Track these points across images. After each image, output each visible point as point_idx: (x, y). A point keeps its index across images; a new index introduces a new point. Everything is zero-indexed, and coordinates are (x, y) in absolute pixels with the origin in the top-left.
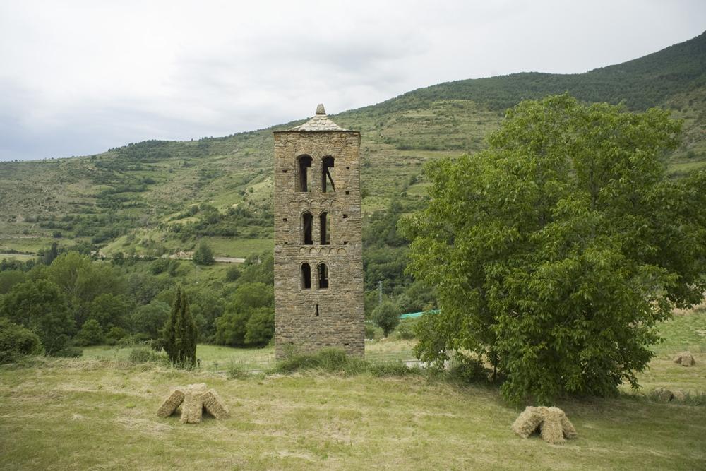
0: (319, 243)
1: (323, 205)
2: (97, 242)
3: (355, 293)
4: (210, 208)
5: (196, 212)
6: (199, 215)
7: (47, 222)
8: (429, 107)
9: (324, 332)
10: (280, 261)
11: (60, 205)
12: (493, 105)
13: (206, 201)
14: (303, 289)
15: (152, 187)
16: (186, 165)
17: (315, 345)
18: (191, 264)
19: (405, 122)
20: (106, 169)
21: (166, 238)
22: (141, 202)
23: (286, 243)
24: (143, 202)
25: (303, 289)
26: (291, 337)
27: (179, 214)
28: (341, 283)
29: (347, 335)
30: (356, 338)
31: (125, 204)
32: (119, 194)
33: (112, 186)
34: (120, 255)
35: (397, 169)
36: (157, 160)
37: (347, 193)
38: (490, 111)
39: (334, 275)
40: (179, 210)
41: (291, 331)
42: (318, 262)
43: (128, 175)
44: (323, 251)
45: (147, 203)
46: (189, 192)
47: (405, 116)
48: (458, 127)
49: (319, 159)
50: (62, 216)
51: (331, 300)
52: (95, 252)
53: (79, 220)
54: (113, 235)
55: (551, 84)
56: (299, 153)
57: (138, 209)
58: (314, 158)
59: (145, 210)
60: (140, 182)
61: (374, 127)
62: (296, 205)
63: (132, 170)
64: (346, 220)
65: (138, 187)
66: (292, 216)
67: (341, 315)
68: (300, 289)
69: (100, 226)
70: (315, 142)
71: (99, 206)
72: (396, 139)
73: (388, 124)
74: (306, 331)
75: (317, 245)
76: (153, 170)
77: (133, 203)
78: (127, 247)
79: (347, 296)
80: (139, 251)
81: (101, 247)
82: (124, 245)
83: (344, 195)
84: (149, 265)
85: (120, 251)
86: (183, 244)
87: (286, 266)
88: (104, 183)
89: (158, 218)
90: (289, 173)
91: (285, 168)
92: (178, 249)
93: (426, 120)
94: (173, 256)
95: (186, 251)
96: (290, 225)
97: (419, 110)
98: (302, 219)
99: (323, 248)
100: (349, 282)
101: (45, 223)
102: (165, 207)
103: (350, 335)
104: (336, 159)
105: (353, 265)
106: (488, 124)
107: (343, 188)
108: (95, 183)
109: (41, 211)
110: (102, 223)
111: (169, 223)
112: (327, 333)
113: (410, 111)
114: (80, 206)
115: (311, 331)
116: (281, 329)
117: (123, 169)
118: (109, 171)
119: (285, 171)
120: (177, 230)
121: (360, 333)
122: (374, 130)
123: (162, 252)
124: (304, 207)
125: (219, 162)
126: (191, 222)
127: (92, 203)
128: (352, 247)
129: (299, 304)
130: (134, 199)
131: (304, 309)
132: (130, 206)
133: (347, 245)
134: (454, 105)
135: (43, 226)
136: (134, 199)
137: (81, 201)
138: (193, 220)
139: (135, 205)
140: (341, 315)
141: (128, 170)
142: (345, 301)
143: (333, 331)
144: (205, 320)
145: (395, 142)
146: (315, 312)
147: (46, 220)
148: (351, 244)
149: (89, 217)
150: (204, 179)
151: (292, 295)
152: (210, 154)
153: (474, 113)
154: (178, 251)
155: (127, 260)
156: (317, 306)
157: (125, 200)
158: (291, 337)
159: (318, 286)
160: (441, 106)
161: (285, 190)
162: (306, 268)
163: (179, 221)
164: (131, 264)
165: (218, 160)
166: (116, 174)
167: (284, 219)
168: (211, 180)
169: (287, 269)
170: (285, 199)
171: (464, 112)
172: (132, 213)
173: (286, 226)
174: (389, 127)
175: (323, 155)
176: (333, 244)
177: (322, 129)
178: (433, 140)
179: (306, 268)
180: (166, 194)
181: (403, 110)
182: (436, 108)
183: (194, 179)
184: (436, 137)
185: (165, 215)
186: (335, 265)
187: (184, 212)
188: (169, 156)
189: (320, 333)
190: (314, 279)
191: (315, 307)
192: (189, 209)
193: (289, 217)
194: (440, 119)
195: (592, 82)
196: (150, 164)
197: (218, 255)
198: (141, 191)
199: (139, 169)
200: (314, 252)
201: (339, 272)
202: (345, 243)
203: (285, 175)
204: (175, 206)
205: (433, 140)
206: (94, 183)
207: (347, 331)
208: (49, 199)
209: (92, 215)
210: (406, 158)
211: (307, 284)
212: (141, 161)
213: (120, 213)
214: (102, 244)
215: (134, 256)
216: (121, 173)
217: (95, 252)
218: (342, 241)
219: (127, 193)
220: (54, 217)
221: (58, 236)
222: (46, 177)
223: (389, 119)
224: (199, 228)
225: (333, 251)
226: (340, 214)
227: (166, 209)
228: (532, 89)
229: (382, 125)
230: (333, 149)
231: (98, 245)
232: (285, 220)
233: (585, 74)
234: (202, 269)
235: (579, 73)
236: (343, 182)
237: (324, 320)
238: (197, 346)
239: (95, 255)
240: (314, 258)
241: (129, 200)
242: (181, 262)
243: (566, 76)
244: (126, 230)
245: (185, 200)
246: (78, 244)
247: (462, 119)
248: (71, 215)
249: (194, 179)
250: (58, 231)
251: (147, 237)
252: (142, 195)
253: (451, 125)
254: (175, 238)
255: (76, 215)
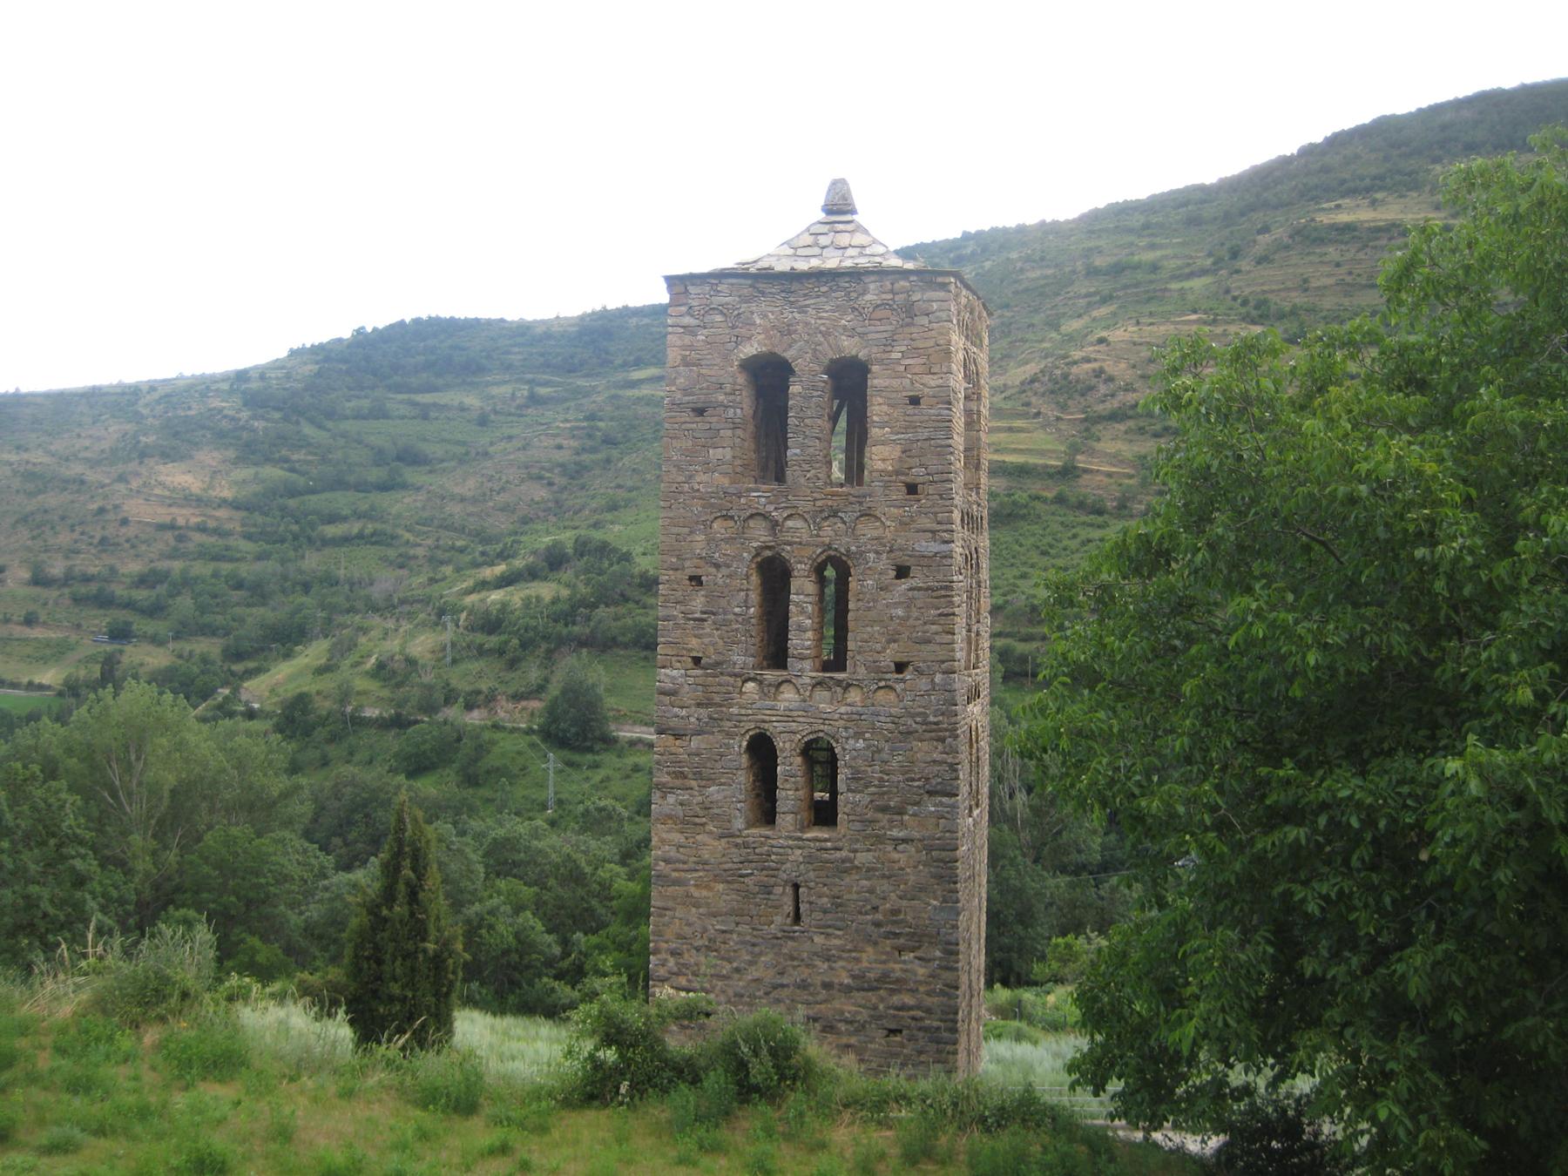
0: (807, 665)
2: (239, 656)
3: (930, 849)
4: (604, 549)
5: (561, 563)
6: (567, 575)
7: (93, 588)
8: (1416, 186)
9: (818, 980)
11: (129, 531)
13: (596, 526)
14: (749, 825)
15: (411, 475)
16: (534, 400)
18: (533, 745)
19: (1321, 241)
20: (277, 415)
21: (457, 655)
22: (379, 526)
24: (388, 528)
25: (749, 825)
27: (500, 569)
28: (884, 809)
30: (929, 1011)
31: (331, 531)
32: (314, 498)
33: (292, 470)
34: (301, 702)
36: (440, 382)
37: (912, 489)
39: (855, 777)
40: (503, 556)
42: (804, 730)
43: (344, 435)
45: (400, 532)
46: (540, 493)
47: (1324, 219)
50: (134, 567)
51: (845, 868)
52: (227, 691)
53: (186, 582)
54: (287, 638)
56: (750, 350)
57: (374, 549)
58: (798, 365)
59: (392, 553)
60: (380, 458)
63: (358, 416)
64: (904, 585)
65: (375, 474)
66: (717, 566)
67: (877, 924)
68: (739, 823)
69: (248, 605)
70: (802, 309)
71: (248, 537)
72: (1287, 307)
73: (1258, 250)
74: (754, 973)
75: (805, 670)
76: (425, 417)
77: (356, 528)
78: (328, 675)
80: (365, 693)
81: (250, 674)
82: (321, 671)
83: (899, 494)
84: (392, 742)
85: (305, 689)
86: (509, 675)
87: (696, 743)
88: (267, 460)
89: (432, 581)
90: (712, 419)
92: (493, 690)
94: (476, 713)
95: (517, 697)
97: (1379, 196)
98: (755, 579)
99: (819, 683)
100: (911, 810)
101: (83, 590)
102: (459, 543)
103: (908, 1000)
105: (925, 746)
107: (897, 473)
108: (239, 461)
109: (78, 552)
110: (258, 592)
111: (469, 600)
112: (827, 986)
113: (1346, 202)
114: (191, 534)
115: (769, 976)
116: (671, 962)
117: (330, 415)
118: (286, 419)
119: (700, 412)
120: (491, 624)
122: (1204, 272)
123: (439, 696)
124: (759, 534)
125: (645, 391)
126: (538, 598)
127: (228, 526)
128: (923, 684)
129: (731, 877)
130: (359, 516)
131: (747, 895)
132: (346, 540)
133: (908, 675)
135: (77, 600)
136: (359, 516)
137: (195, 520)
138: (546, 591)
139: (360, 536)
141: (347, 418)
144: (549, 938)
145: (1281, 316)
146: (789, 908)
147: (87, 579)
149: (215, 575)
150: (594, 450)
151: (711, 847)
152: (618, 361)
154: (490, 699)
155: (323, 721)
156: (796, 887)
157: (332, 519)
162: (762, 750)
163: (496, 596)
164: (333, 738)
165: (641, 382)
166: (308, 430)
167: (691, 578)
168: (615, 453)
172: (349, 564)
173: (698, 602)
174: (1262, 260)
176: (857, 668)
177: (832, 264)
179: (762, 750)
180: (463, 500)
181: (1314, 199)
183: (560, 447)
185: (458, 570)
186: (861, 744)
187: (519, 563)
188: (481, 370)
190: (791, 793)
191: (789, 890)
192: (534, 553)
193: (708, 574)
196: (419, 398)
197: (621, 718)
198: (384, 487)
199: (379, 413)
200: (788, 696)
201: (875, 772)
202: (900, 667)
203: (699, 425)
204: (487, 540)
206: (237, 462)
207: (899, 985)
208: (102, 510)
209: (226, 567)
211: (767, 813)
212: (389, 388)
213: (312, 561)
214: (251, 665)
215: (349, 709)
216: (320, 427)
217: (227, 691)
218: (888, 658)
219: (338, 495)
220: (113, 570)
221: (120, 634)
222: (99, 439)
223: (1265, 230)
224: (568, 617)
225: (854, 696)
226: (884, 564)
227: (462, 550)
229: (1235, 254)
231: (238, 668)
232: (696, 580)
234: (570, 764)
236: (897, 453)
237: (818, 939)
238: (456, 1014)
239: (226, 698)
240: (788, 717)
241: (345, 519)
242: (498, 736)
244: (329, 620)
245: (525, 521)
246: (180, 662)
248: (163, 565)
249: (560, 447)
250: (122, 615)
251: (393, 645)
252: (382, 500)
254: (481, 652)
255: (177, 566)
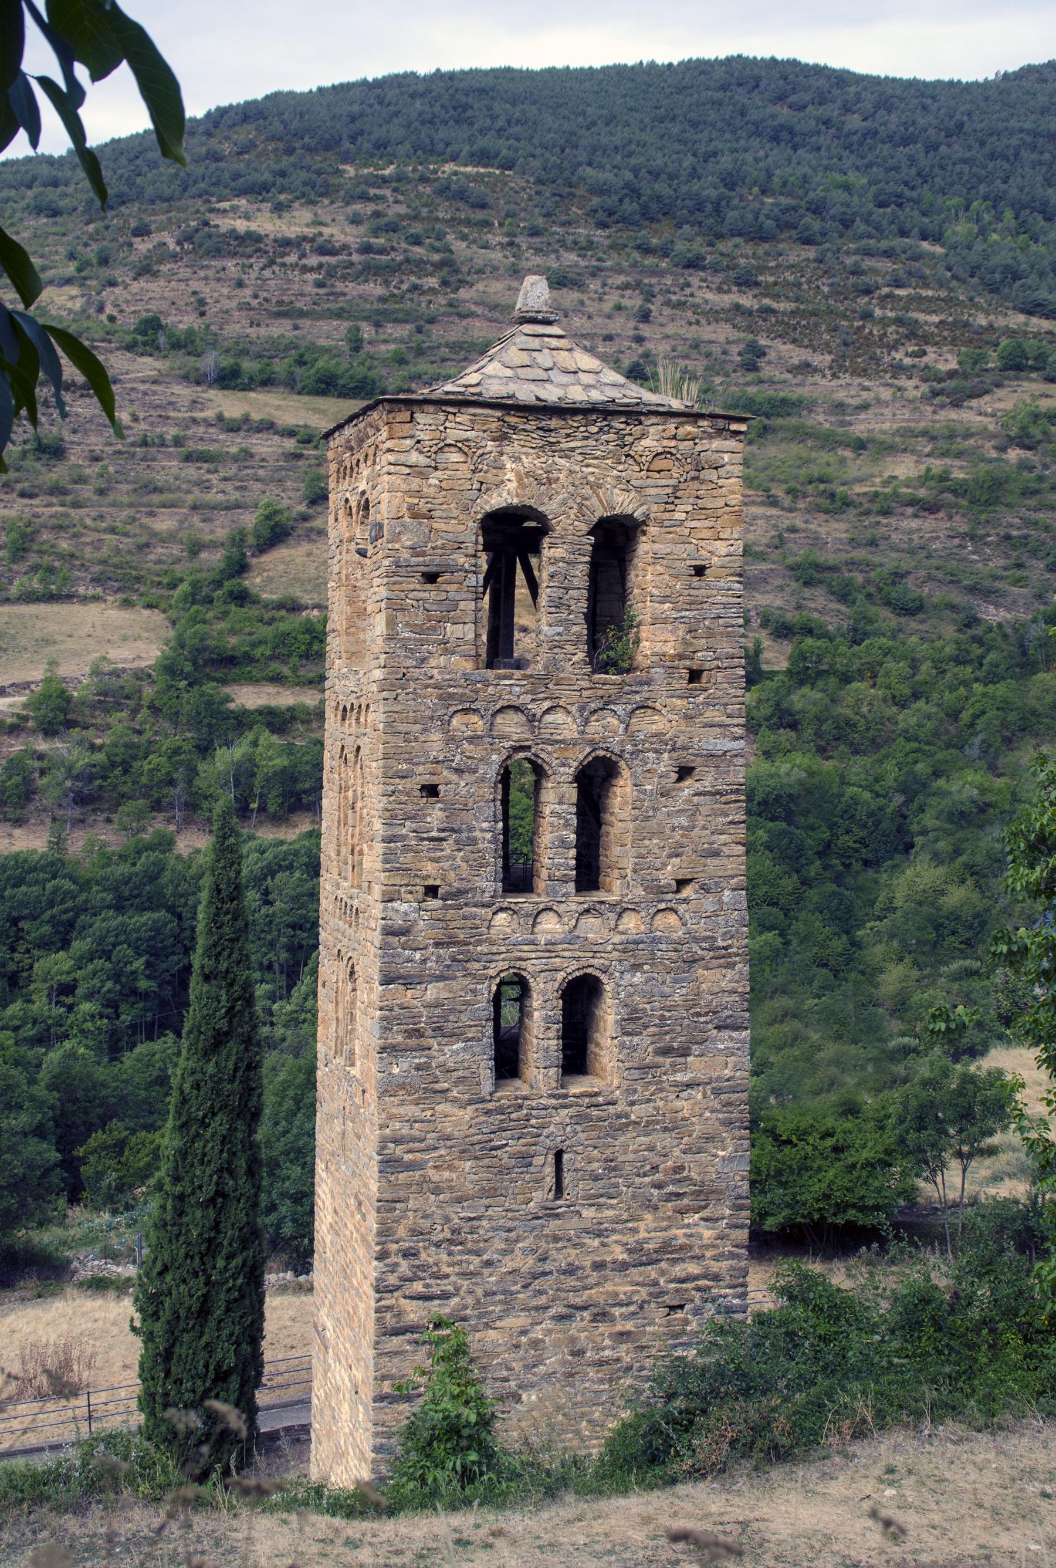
1: (594, 727)
3: (717, 1092)
8: (327, 191)
10: (409, 968)
12: (611, 201)
17: (548, 1324)
19: (217, 252)
23: (432, 891)
26: (445, 1296)
29: (678, 1270)
30: (716, 1278)
35: (191, 471)
37: (695, 676)
38: (603, 225)
41: (447, 1270)
42: (570, 968)
44: (590, 921)
47: (225, 224)
48: (463, 294)
49: (585, 528)
55: (854, 122)
56: (496, 501)
61: (71, 269)
62: (478, 724)
64: (689, 786)
66: (459, 771)
67: (659, 1186)
79: (684, 1106)
90: (448, 587)
91: (431, 561)
93: (323, 251)
96: (450, 811)
103: (693, 1268)
104: (653, 530)
106: (594, 285)
107: (681, 657)
112: (598, 1266)
116: (404, 1267)
119: (431, 578)
121: (732, 1256)
128: (709, 904)
134: (444, 191)
140: (659, 1186)
142: (674, 1126)
143: (623, 1256)
146: (550, 1181)
148: (705, 889)
153: (535, 232)
156: (559, 1155)
158: (445, 1296)
159: (563, 1067)
160: (387, 192)
161: (433, 662)
167: (423, 788)
169: (437, 1005)
170: (431, 698)
171: (486, 224)
173: (435, 816)
175: (600, 513)
178: (356, 345)
182: (364, 197)
184: (367, 331)
189: (571, 1270)
191: (551, 1158)
194: (381, 251)
195: (1013, 123)
201: (652, 1009)
202: (681, 883)
203: (431, 594)
205: (356, 345)
210: (233, 427)
218: (667, 876)
223: (142, 232)
226: (666, 764)
228: (775, 139)
230: (639, 489)
232: (431, 791)
233: (986, 85)
235: (967, 78)
243: (914, 85)
247: (482, 256)
253: (433, 282)
